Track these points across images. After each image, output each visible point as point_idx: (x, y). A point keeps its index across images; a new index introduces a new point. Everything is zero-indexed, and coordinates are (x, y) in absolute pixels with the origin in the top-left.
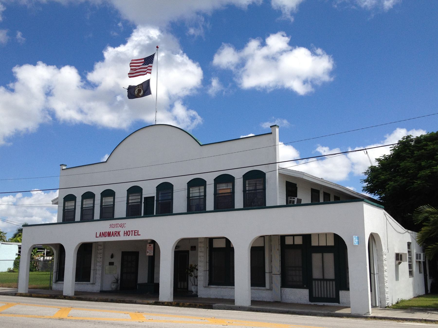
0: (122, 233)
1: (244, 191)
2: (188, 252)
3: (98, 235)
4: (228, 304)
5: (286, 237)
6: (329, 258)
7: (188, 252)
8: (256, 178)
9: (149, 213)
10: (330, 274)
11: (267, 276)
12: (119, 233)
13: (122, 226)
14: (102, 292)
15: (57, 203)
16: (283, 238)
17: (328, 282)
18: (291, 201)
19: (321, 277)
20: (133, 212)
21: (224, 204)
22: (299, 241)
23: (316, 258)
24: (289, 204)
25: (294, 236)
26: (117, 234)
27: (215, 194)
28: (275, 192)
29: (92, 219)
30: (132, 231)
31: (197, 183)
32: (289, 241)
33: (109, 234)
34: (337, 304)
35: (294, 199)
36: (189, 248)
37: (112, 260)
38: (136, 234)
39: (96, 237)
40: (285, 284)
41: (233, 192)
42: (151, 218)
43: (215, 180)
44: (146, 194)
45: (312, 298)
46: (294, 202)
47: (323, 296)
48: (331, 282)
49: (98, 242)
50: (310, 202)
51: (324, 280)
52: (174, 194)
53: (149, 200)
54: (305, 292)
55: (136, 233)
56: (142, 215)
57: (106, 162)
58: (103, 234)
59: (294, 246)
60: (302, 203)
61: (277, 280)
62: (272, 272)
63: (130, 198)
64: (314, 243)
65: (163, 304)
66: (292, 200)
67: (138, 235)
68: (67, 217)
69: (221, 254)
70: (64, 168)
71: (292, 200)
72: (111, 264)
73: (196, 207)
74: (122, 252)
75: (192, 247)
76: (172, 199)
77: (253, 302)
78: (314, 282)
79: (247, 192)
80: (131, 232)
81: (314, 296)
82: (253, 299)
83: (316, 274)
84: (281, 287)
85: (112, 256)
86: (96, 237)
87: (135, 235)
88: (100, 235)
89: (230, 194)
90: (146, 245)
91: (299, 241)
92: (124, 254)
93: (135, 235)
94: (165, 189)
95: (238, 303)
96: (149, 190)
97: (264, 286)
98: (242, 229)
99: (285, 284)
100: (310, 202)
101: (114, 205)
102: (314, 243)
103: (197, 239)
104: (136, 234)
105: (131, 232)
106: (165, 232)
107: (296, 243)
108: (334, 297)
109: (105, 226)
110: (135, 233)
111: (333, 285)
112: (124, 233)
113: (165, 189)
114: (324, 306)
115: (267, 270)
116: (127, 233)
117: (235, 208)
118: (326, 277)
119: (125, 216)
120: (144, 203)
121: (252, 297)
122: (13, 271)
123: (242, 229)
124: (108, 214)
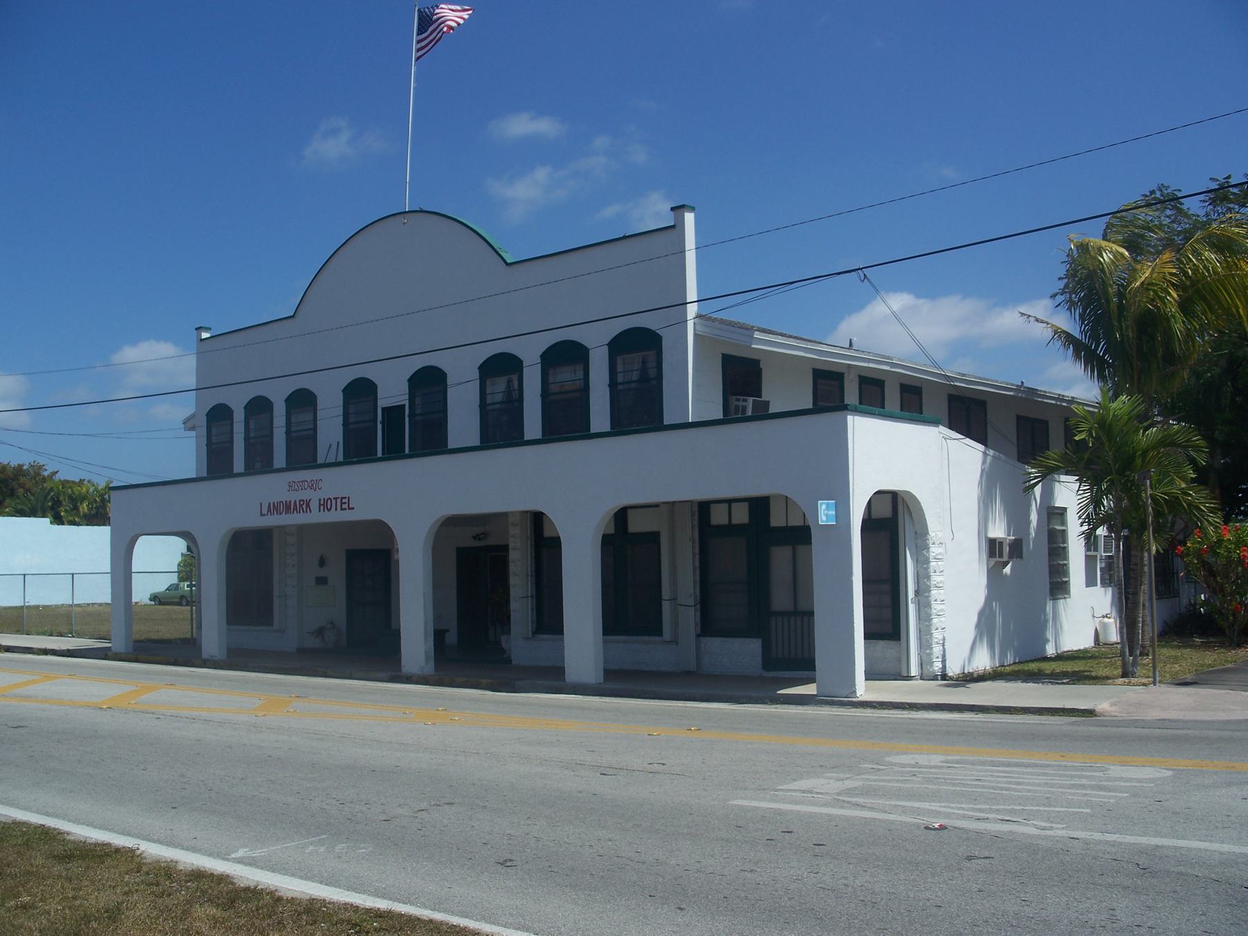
0: (314, 505)
1: (613, 384)
3: (265, 512)
4: (551, 677)
5: (712, 506)
8: (640, 348)
9: (394, 451)
11: (666, 607)
12: (308, 505)
13: (314, 486)
14: (302, 651)
15: (192, 429)
16: (704, 508)
18: (737, 407)
20: (358, 448)
21: (566, 421)
22: (741, 515)
24: (731, 416)
25: (730, 501)
27: (545, 394)
28: (692, 388)
30: (336, 499)
31: (501, 367)
32: (719, 517)
33: (288, 508)
35: (745, 401)
37: (321, 573)
38: (345, 506)
40: (708, 627)
41: (586, 389)
42: (579, 442)
43: (542, 356)
46: (744, 409)
49: (284, 527)
50: (608, 429)
52: (451, 393)
53: (393, 413)
54: (754, 646)
55: (344, 503)
56: (380, 454)
58: (275, 508)
59: (730, 530)
60: (772, 410)
61: (690, 618)
62: (675, 599)
63: (214, 431)
65: (409, 679)
66: (741, 403)
68: (217, 463)
69: (368, 560)
70: (205, 335)
71: (741, 403)
72: (321, 581)
73: (501, 429)
74: (458, 549)
76: (445, 410)
77: (609, 674)
79: (620, 387)
84: (698, 636)
85: (322, 562)
88: (269, 510)
91: (741, 515)
92: (353, 556)
94: (429, 382)
95: (572, 675)
96: (393, 390)
97: (659, 632)
98: (578, 488)
99: (708, 627)
100: (608, 429)
101: (315, 429)
103: (504, 515)
104: (345, 506)
106: (411, 501)
107: (734, 522)
109: (275, 487)
110: (342, 503)
113: (429, 382)
115: (666, 593)
116: (325, 505)
117: (450, 447)
119: (478, 443)
120: (383, 423)
121: (606, 661)
122: (183, 600)
123: (578, 488)
124: (303, 453)
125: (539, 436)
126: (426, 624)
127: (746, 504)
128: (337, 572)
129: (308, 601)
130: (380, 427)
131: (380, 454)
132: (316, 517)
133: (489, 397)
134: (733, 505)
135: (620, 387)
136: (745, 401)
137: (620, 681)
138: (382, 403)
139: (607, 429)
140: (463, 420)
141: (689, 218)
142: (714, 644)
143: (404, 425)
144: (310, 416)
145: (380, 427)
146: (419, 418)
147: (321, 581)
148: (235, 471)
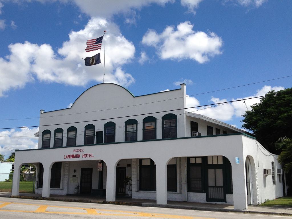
0: (81, 156)
1: (163, 127)
2: (125, 168)
3: (65, 157)
4: (152, 203)
6: (220, 172)
7: (125, 168)
9: (99, 142)
10: (220, 182)
11: (178, 184)
12: (79, 156)
14: (68, 195)
16: (188, 159)
17: (219, 188)
18: (194, 134)
19: (213, 185)
20: (89, 142)
22: (199, 161)
23: (211, 172)
24: (193, 136)
25: (196, 157)
26: (78, 156)
27: (144, 129)
29: (61, 147)
30: (88, 154)
31: (132, 122)
32: (193, 161)
33: (73, 156)
34: (224, 203)
36: (126, 166)
37: (75, 174)
38: (90, 156)
39: (64, 158)
40: (190, 190)
41: (155, 129)
42: (199, 138)
44: (97, 129)
45: (208, 199)
47: (215, 198)
48: (221, 189)
51: (216, 187)
53: (99, 134)
55: (91, 155)
56: (95, 143)
57: (71, 108)
58: (68, 157)
59: (196, 164)
61: (185, 187)
62: (181, 182)
63: (87, 132)
64: (210, 162)
65: (109, 203)
66: (195, 133)
67: (92, 157)
68: (45, 145)
69: (147, 170)
70: (43, 112)
71: (195, 133)
72: (74, 176)
73: (131, 138)
75: (128, 165)
76: (115, 133)
77: (169, 202)
78: (209, 188)
80: (87, 155)
81: (209, 197)
82: (168, 200)
83: (211, 183)
84: (187, 192)
85: (75, 171)
86: (64, 158)
87: (90, 157)
89: (153, 130)
90: (97, 164)
91: (199, 161)
92: (83, 170)
93: (90, 157)
94: (110, 126)
95: (158, 202)
96: (100, 127)
98: (161, 153)
99: (190, 190)
102: (210, 162)
104: (90, 156)
105: (87, 155)
106: (110, 155)
107: (197, 163)
108: (223, 198)
109: (70, 151)
110: (90, 155)
111: (222, 190)
112: (83, 156)
113: (110, 126)
114: (216, 204)
115: (178, 180)
116: (84, 156)
118: (218, 185)
121: (168, 199)
123: (161, 153)
125: (142, 139)
126: (114, 188)
127: (201, 158)
128: (78, 174)
129: (70, 183)
130: (95, 137)
131: (95, 143)
132: (81, 159)
133: (127, 130)
134: (197, 158)
135: (69, 138)
136: (196, 133)
137: (172, 204)
138: (96, 131)
139: (53, 147)
140: (120, 134)
141: (185, 87)
142: (192, 194)
143: (107, 136)
144: (153, 124)
145: (95, 137)
146: (107, 135)
147: (74, 176)
148: (51, 147)
